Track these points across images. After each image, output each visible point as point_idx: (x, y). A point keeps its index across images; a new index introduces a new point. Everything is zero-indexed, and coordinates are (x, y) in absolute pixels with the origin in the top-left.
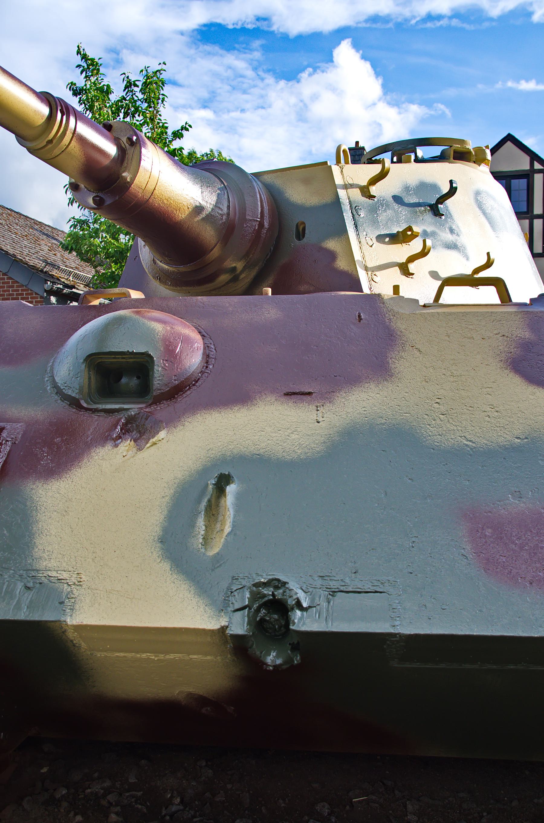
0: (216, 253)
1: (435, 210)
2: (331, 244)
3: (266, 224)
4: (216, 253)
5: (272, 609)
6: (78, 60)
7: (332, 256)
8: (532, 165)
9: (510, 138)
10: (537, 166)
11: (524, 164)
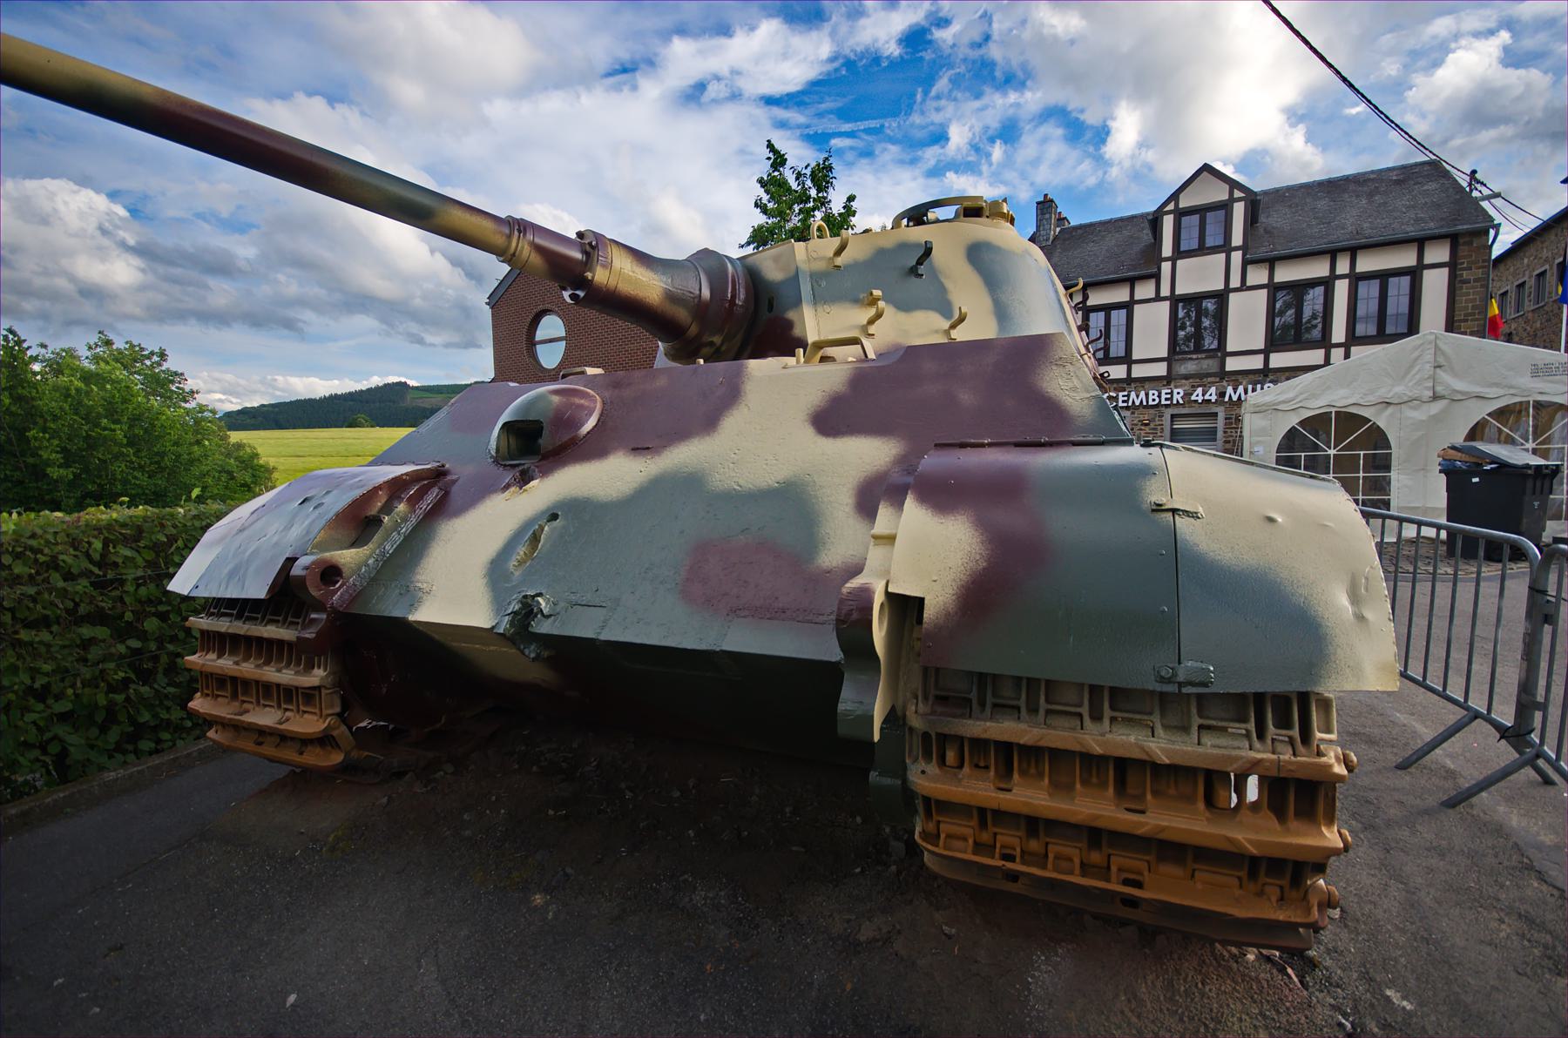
0: (694, 330)
4: (694, 330)
5: (528, 611)
6: (767, 153)
7: (789, 325)
8: (1231, 193)
9: (1206, 168)
10: (1237, 194)
11: (1220, 194)
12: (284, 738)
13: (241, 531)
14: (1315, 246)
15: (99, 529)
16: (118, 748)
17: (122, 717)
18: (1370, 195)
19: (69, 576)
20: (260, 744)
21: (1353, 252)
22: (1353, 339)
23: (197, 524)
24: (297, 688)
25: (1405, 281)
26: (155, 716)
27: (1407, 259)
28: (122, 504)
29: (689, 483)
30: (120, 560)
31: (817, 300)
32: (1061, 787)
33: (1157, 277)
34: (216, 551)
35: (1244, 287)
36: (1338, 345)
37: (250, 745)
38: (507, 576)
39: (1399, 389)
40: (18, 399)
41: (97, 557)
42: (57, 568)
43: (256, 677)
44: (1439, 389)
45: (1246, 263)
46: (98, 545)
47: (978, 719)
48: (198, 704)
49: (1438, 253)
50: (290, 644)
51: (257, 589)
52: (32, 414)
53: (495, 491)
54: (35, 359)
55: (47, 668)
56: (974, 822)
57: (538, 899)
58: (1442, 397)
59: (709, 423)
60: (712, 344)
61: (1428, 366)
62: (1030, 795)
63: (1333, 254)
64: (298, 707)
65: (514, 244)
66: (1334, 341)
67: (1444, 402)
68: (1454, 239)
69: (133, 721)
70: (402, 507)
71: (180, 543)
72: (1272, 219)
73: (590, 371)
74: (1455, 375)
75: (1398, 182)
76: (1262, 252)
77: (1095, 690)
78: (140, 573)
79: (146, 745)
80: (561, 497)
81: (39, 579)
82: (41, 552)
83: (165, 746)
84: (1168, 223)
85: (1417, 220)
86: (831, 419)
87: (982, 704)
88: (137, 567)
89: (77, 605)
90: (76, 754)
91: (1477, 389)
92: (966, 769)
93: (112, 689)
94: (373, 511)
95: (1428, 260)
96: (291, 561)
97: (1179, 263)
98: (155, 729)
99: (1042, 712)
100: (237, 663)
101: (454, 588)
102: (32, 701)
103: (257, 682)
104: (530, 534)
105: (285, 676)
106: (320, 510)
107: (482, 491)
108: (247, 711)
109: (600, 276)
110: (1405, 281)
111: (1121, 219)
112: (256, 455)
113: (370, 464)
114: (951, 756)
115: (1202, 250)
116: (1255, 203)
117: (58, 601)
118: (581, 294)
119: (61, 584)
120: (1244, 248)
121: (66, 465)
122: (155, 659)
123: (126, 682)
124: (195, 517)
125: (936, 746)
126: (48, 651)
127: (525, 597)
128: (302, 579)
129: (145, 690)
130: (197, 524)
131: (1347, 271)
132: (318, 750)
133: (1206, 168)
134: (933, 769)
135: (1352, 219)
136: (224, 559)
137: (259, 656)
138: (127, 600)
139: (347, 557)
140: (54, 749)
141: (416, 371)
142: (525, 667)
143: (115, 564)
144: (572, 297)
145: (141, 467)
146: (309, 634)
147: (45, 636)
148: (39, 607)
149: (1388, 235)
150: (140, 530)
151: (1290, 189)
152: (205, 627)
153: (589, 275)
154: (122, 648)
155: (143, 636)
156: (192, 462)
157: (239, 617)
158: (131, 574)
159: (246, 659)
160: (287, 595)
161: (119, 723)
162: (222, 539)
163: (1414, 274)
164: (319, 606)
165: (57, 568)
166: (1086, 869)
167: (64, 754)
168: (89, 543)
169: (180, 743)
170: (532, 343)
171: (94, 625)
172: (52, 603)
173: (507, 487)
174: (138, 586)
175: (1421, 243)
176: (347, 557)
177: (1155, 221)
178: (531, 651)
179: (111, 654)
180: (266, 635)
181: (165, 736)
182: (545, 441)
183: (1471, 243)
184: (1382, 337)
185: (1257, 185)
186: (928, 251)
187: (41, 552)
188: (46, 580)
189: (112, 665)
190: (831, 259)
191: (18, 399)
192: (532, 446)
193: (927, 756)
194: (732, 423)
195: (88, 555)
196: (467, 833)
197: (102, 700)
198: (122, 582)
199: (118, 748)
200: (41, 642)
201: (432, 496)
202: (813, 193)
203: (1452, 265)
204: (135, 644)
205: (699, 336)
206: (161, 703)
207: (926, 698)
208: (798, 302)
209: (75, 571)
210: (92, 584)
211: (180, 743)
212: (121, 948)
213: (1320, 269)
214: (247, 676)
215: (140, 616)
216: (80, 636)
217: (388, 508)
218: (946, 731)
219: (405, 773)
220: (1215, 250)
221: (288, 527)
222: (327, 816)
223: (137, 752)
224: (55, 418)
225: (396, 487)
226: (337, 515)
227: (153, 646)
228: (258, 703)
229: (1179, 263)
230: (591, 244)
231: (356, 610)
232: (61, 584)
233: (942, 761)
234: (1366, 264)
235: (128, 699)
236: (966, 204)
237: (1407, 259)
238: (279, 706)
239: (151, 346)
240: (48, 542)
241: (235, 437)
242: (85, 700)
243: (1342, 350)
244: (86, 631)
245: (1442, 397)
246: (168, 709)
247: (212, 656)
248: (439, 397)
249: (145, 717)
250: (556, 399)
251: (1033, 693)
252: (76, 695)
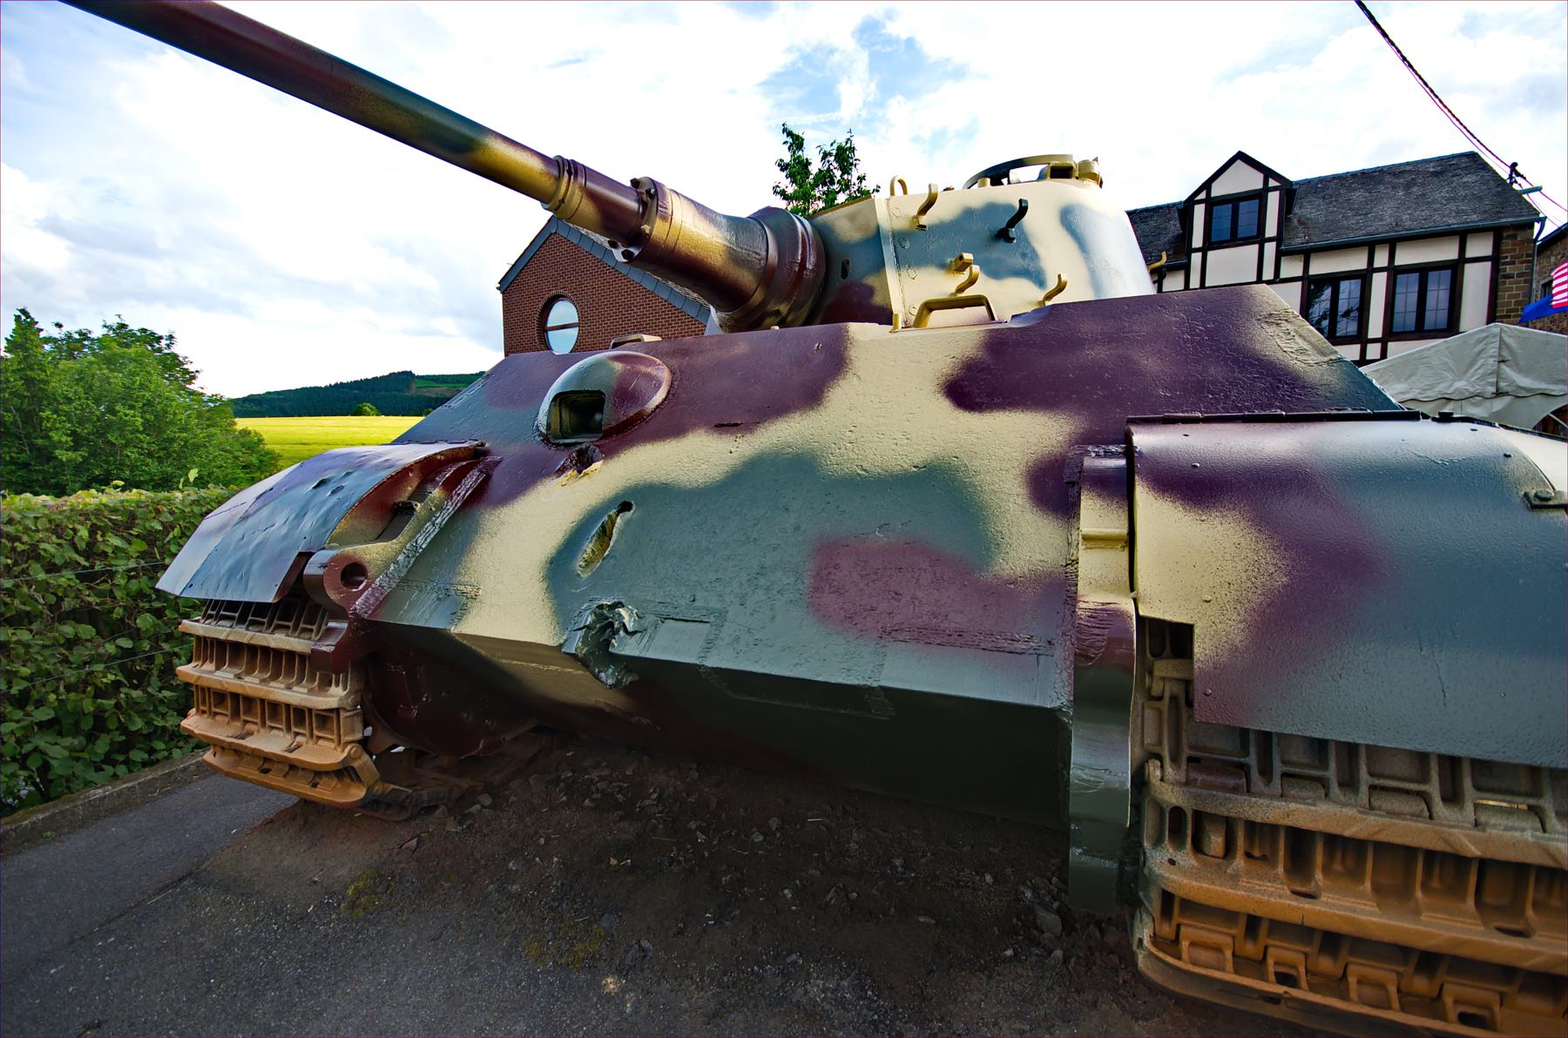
0: (758, 297)
1: (1003, 235)
2: (871, 280)
3: (809, 266)
4: (758, 297)
6: (784, 137)
7: (871, 291)
8: (1266, 182)
9: (1241, 156)
10: (1272, 183)
11: (1255, 181)
12: (293, 767)
13: (245, 518)
14: (1351, 236)
15: (85, 515)
16: (108, 760)
17: (112, 725)
18: (1407, 186)
19: (52, 568)
20: (266, 771)
21: (1392, 244)
22: (1391, 333)
23: (196, 509)
24: (310, 710)
25: (1447, 274)
26: (149, 723)
27: (1448, 252)
28: (116, 487)
29: (799, 468)
30: (109, 550)
31: (900, 264)
32: (1393, 893)
33: (1186, 269)
34: (216, 541)
35: (1277, 280)
36: (1374, 341)
37: (254, 774)
38: (573, 578)
39: (1460, 384)
40: (29, 382)
41: (82, 546)
42: (38, 558)
43: (261, 695)
44: (1502, 384)
45: (1279, 255)
46: (84, 533)
47: (1260, 795)
48: (193, 722)
49: (1480, 247)
50: (302, 656)
51: (266, 593)
52: (35, 393)
53: (548, 475)
54: (48, 340)
55: (26, 671)
56: (1239, 930)
57: (611, 984)
58: (1506, 394)
59: (811, 396)
60: (778, 313)
61: (1491, 361)
62: (1344, 905)
63: (1371, 246)
64: (315, 735)
65: (563, 188)
66: (1371, 335)
67: (1506, 400)
68: (1498, 233)
69: (123, 729)
70: (436, 493)
71: (177, 531)
72: (1306, 210)
73: (647, 338)
74: (1520, 371)
75: (1436, 174)
76: (1298, 241)
77: (1451, 764)
78: (132, 564)
79: (138, 756)
80: (632, 483)
81: (17, 569)
82: (19, 539)
83: (159, 756)
84: (1199, 211)
85: (1458, 212)
86: (969, 389)
87: (1266, 772)
88: (129, 558)
89: (60, 599)
90: (58, 768)
91: (1543, 386)
92: (1239, 862)
93: (99, 693)
94: (403, 497)
95: (1471, 252)
96: (305, 556)
97: (1211, 254)
98: (148, 737)
99: (1364, 789)
100: (239, 677)
101: (505, 593)
102: (10, 709)
103: (262, 701)
104: (596, 527)
105: (297, 694)
106: (339, 495)
107: (531, 474)
108: (250, 734)
109: (657, 229)
110: (1447, 274)
111: (1147, 210)
112: (260, 441)
113: (395, 442)
114: (1216, 842)
115: (1235, 240)
116: (1290, 192)
117: (38, 596)
118: (636, 252)
119: (42, 576)
120: (1279, 239)
121: (75, 449)
122: (151, 659)
123: (117, 685)
124: (194, 502)
125: (1185, 827)
126: (27, 653)
127: (601, 607)
128: (320, 579)
129: (136, 694)
130: (196, 509)
131: (1385, 264)
132: (334, 782)
134: (1186, 858)
135: (1388, 213)
136: (224, 549)
137: (264, 669)
138: (118, 594)
139: (373, 552)
140: (34, 763)
141: (428, 361)
142: (598, 690)
143: (105, 554)
144: (626, 254)
145: (150, 455)
146: (327, 646)
147: (25, 636)
148: (17, 602)
149: (1428, 226)
150: (132, 517)
151: (1321, 180)
152: (201, 633)
153: (647, 228)
154: (110, 648)
155: (136, 635)
156: (197, 447)
157: (241, 621)
158: (121, 565)
159: (250, 671)
160: (299, 600)
161: (108, 732)
162: (221, 528)
163: (1455, 269)
164: (339, 613)
165: (38, 558)
166: (1409, 1001)
167: (45, 767)
168: (75, 530)
169: (177, 753)
170: (543, 330)
171: (78, 621)
172: (32, 597)
173: (562, 471)
174: (130, 578)
175: (1462, 236)
176: (373, 552)
177: (1184, 210)
178: (608, 676)
179: (100, 655)
180: (273, 645)
181: (159, 745)
182: (608, 416)
183: (1515, 237)
184: (1420, 331)
185: (1294, 174)
186: (1023, 210)
187: (19, 539)
188: (24, 572)
189: (99, 667)
190: (916, 218)
191: (29, 382)
192: (592, 423)
193: (1177, 837)
194: (840, 395)
195: (74, 546)
196: (515, 888)
197: (88, 706)
198: (112, 575)
199: (108, 760)
200: (19, 642)
201: (471, 481)
202: (838, 173)
203: (1495, 259)
204: (126, 643)
205: (763, 303)
206: (155, 707)
207: (1175, 760)
208: (880, 266)
209: (58, 561)
210: (78, 576)
211: (177, 753)
212: (99, 1025)
213: (1357, 262)
214: (250, 693)
215: (132, 612)
216: (62, 634)
217: (420, 494)
218: (1210, 809)
219: (436, 807)
220: (1247, 241)
221: (301, 515)
222: (345, 861)
223: (127, 762)
224: (69, 401)
225: (428, 468)
226: (361, 501)
227: (146, 645)
228: (264, 724)
229: (1211, 254)
230: (649, 193)
231: (386, 617)
232: (42, 576)
233: (1198, 848)
234: (1404, 257)
235: (118, 706)
236: (1053, 163)
237: (1446, 252)
238: (289, 729)
239: (161, 331)
240: (27, 529)
241: (242, 423)
242: (69, 707)
243: (1378, 346)
244: (68, 629)
245: (1506, 394)
246: (164, 716)
247: (210, 666)
248: (445, 387)
249: (138, 724)
250: (618, 366)
251: (1338, 762)
252: (61, 702)
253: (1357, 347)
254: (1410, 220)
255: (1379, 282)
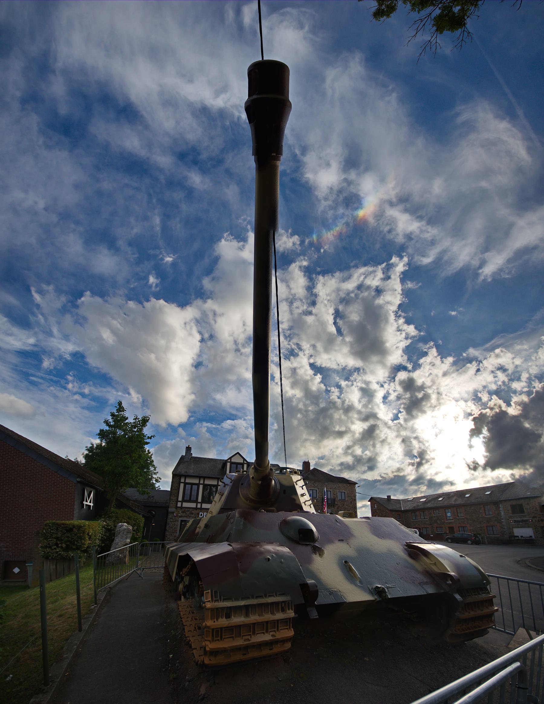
2: (294, 497)
7: (294, 500)
9: (238, 453)
11: (241, 461)
21: (204, 478)
63: (200, 477)
133: (238, 453)
253: (195, 504)
254: (191, 472)
255: (201, 487)
